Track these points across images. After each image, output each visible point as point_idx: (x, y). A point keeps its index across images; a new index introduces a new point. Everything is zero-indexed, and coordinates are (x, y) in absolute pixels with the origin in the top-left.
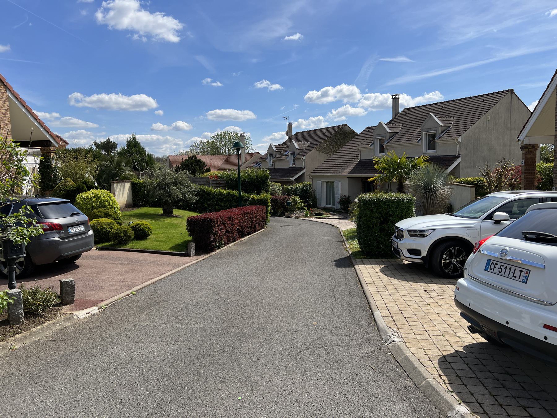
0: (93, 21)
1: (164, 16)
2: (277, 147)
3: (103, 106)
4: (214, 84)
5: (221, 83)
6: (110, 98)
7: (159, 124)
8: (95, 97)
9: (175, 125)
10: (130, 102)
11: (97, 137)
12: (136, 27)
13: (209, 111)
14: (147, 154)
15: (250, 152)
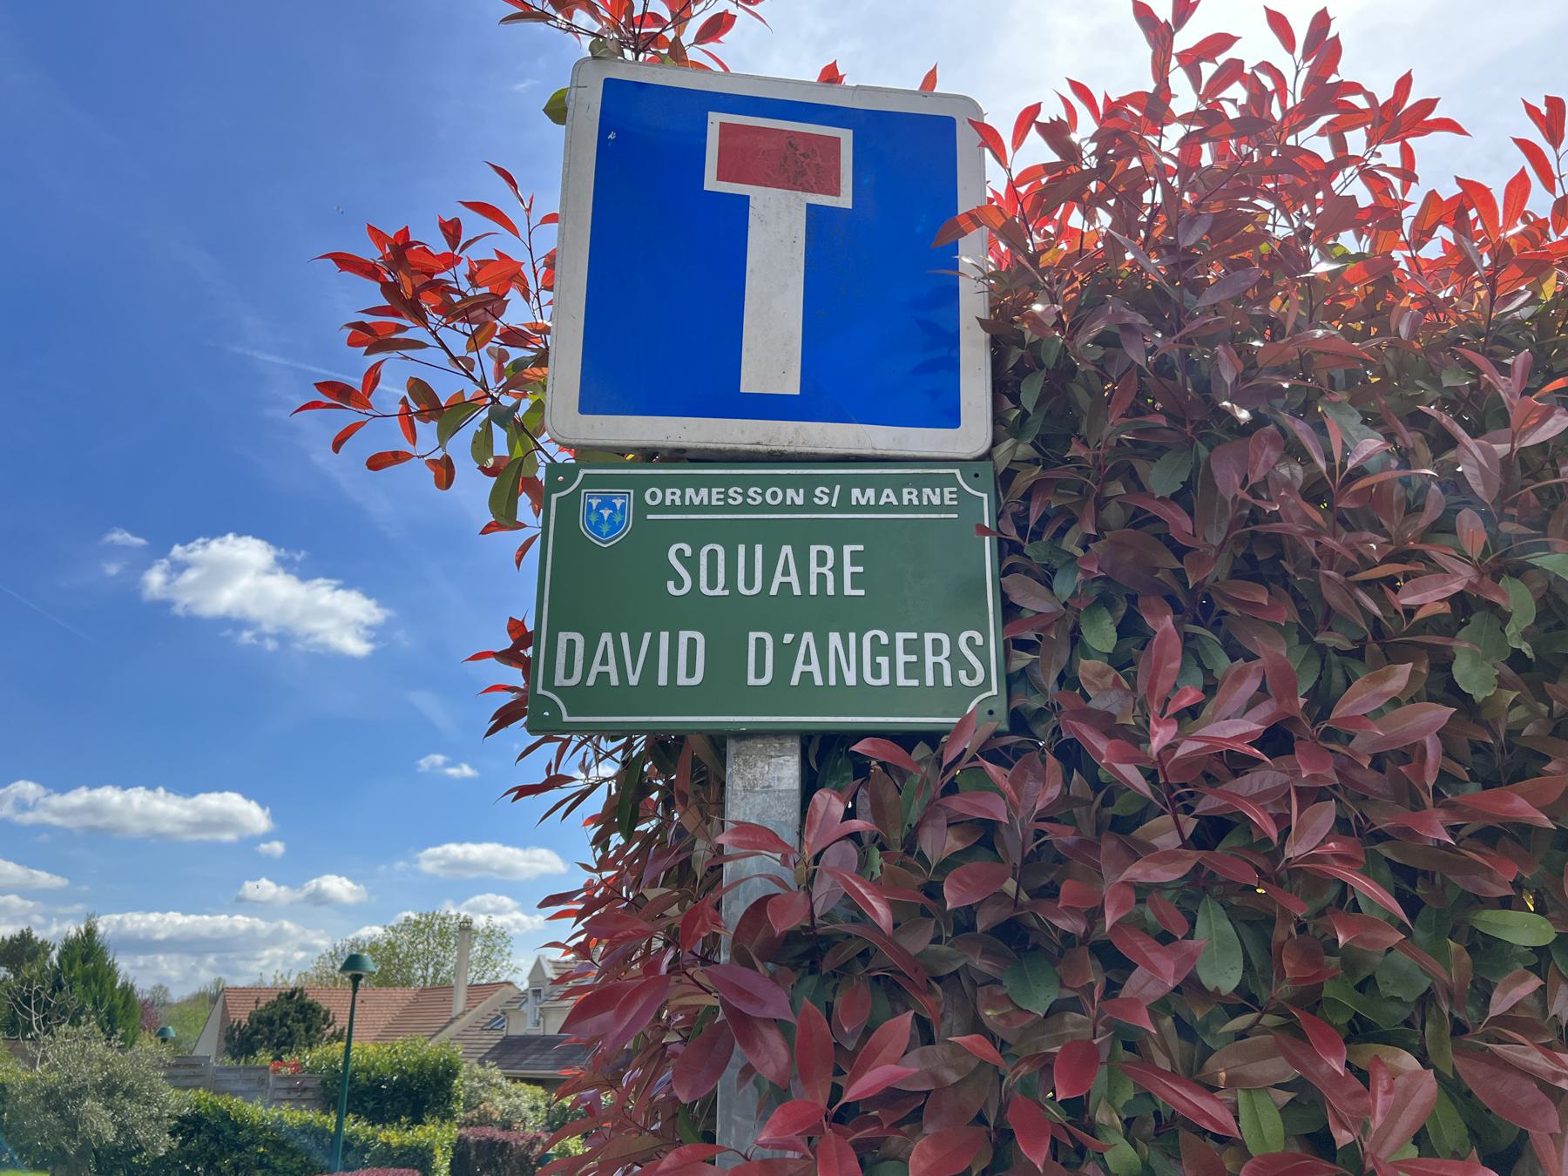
0: (130, 591)
1: (337, 588)
2: (558, 966)
3: (100, 822)
4: (453, 771)
5: (473, 766)
6: (129, 802)
7: (264, 882)
8: (79, 797)
9: (314, 886)
10: (187, 814)
11: (55, 919)
12: (254, 611)
13: (426, 847)
14: (118, 985)
15: (502, 979)
